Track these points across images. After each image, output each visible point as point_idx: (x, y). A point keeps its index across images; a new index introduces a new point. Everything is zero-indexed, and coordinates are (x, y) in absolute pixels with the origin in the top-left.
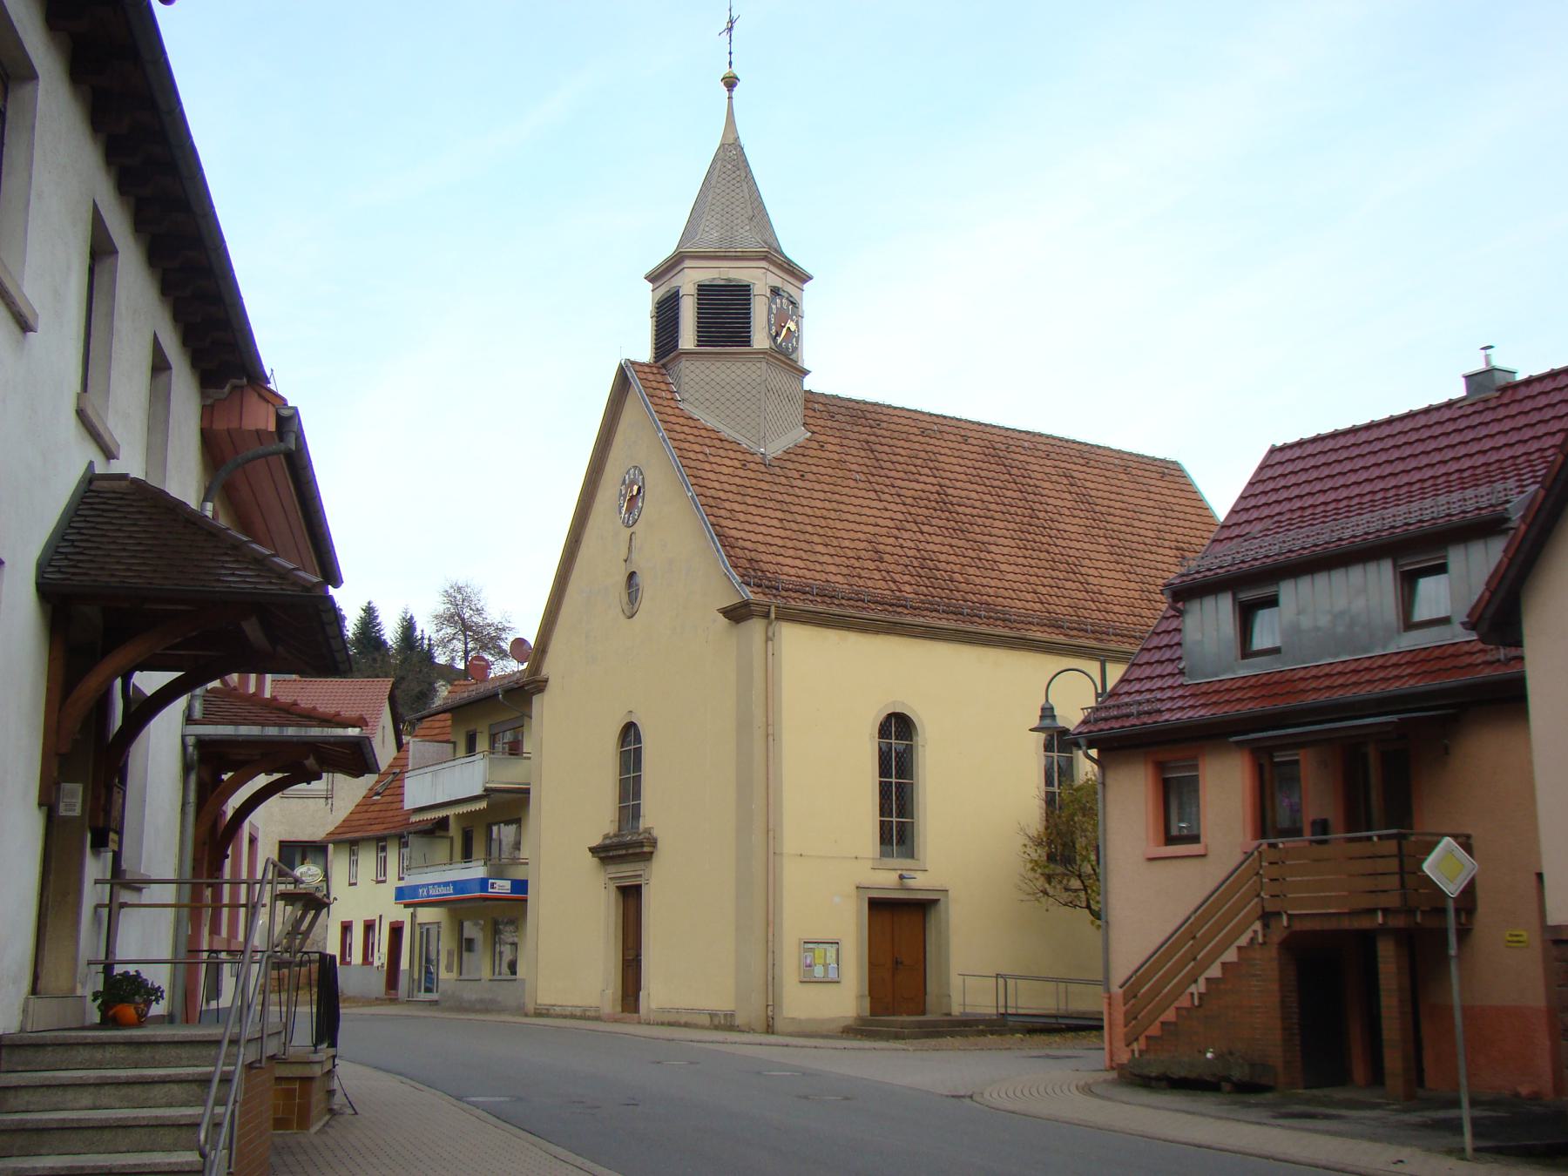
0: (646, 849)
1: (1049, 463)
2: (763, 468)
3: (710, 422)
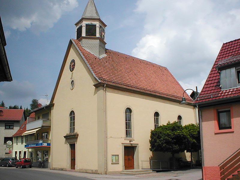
0: (76, 136)
2: (99, 60)
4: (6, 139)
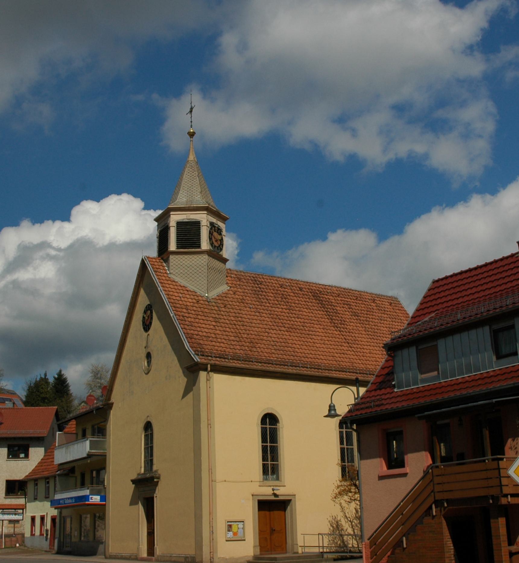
1: (339, 299)
2: (207, 303)
3: (183, 282)
4: (14, 487)
